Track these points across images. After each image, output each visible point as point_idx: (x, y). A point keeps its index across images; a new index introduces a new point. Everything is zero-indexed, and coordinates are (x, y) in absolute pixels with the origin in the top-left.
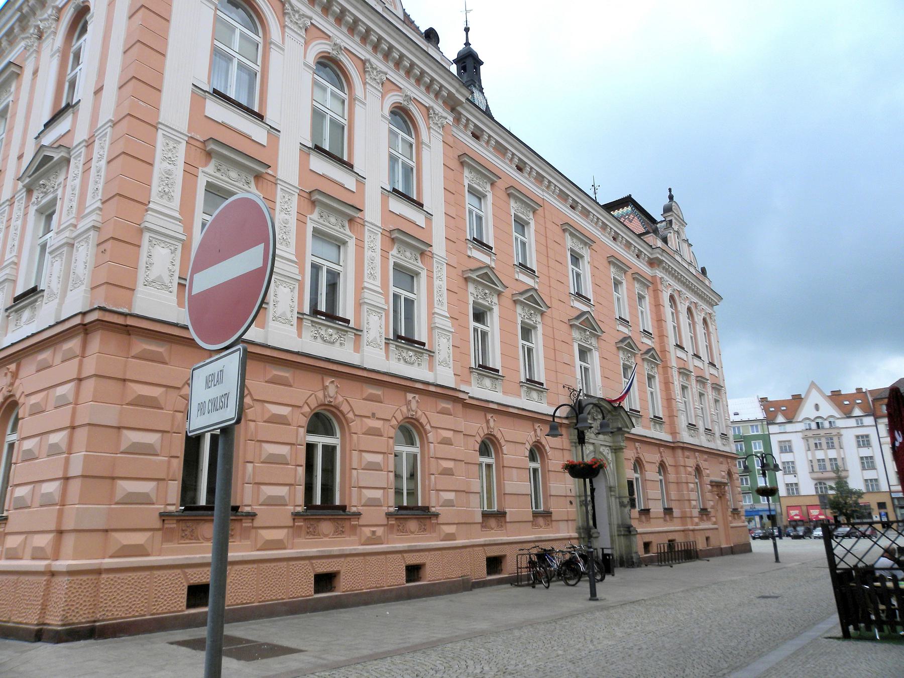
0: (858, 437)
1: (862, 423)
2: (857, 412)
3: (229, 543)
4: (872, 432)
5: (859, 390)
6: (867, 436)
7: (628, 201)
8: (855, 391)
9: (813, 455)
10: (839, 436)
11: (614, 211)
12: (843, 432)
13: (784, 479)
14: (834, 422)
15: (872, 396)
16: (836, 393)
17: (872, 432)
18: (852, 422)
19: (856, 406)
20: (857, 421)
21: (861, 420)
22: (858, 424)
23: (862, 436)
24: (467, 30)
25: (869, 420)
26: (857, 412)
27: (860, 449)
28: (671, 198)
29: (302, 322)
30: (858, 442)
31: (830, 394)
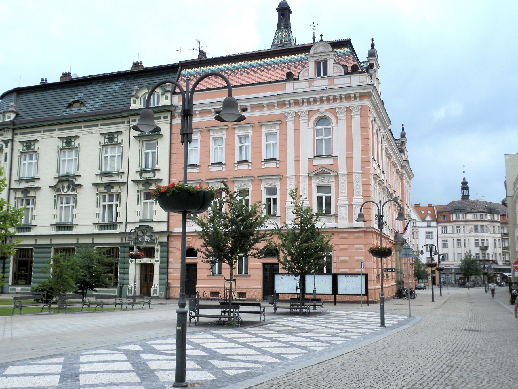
0: (426, 233)
1: (430, 225)
2: (428, 218)
3: (179, 285)
4: (434, 230)
5: (430, 205)
6: (432, 233)
7: (347, 43)
8: (427, 205)
9: (416, 241)
10: (417, 231)
11: (337, 49)
12: (419, 229)
13: (157, 298)
14: (415, 223)
15: (437, 209)
16: (417, 206)
17: (434, 230)
18: (425, 224)
19: (428, 215)
20: (427, 223)
21: (430, 223)
22: (428, 225)
23: (429, 233)
24: (464, 172)
25: (434, 224)
26: (428, 218)
27: (427, 240)
28: (373, 45)
29: (311, 180)
30: (427, 235)
31: (414, 206)
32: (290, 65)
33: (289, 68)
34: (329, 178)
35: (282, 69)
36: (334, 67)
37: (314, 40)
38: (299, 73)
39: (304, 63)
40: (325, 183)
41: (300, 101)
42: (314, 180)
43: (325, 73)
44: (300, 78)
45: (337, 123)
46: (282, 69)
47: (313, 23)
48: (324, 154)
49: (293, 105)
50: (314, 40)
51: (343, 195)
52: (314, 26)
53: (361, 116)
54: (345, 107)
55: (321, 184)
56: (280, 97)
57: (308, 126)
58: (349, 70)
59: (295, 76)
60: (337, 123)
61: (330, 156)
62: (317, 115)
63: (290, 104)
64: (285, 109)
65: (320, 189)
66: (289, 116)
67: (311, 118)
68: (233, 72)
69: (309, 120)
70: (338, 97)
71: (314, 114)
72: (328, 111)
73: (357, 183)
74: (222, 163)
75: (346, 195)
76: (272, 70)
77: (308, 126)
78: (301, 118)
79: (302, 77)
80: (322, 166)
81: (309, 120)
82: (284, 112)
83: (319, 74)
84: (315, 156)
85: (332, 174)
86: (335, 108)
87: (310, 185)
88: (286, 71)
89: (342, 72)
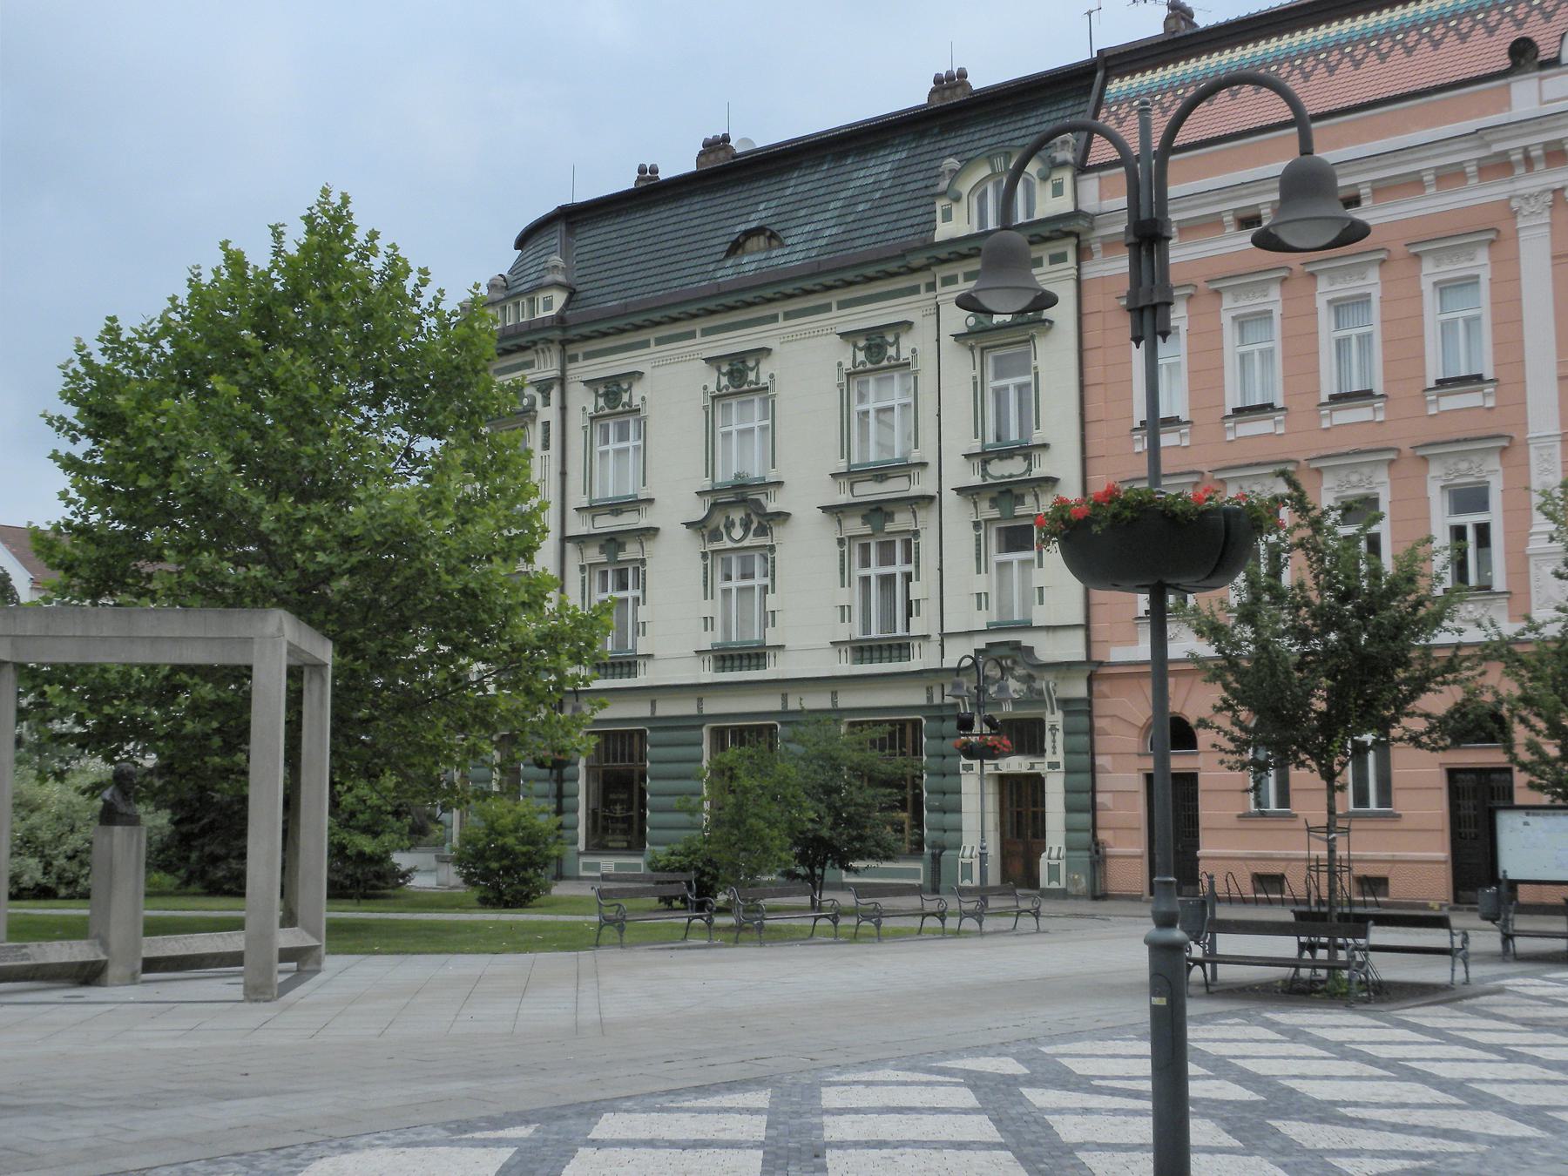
33: (1519, 24)
46: (1491, 31)
59: (1545, 53)
64: (1512, 182)
76: (1452, 38)
88: (1509, 34)
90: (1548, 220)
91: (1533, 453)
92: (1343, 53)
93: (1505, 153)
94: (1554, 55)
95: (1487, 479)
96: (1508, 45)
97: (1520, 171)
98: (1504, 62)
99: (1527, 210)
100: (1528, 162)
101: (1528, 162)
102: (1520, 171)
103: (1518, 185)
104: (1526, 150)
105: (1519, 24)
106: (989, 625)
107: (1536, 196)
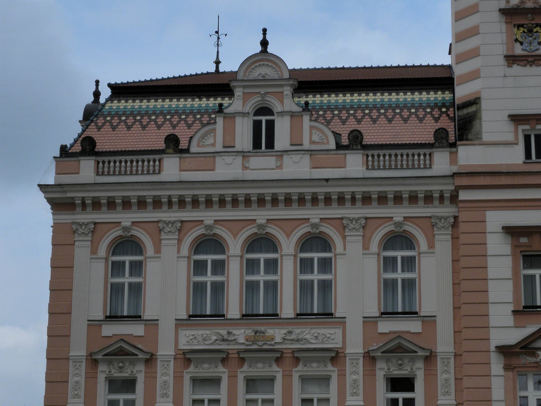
32: (175, 119)
33: (174, 127)
34: (134, 365)
35: (159, 127)
36: (311, 127)
37: (217, 67)
38: (191, 138)
39: (205, 119)
40: (126, 374)
41: (165, 200)
42: (102, 368)
43: (270, 144)
44: (193, 149)
45: (345, 249)
46: (159, 127)
47: (217, 32)
48: (261, 312)
49: (191, 206)
50: (217, 67)
51: (355, 398)
52: (218, 38)
53: (452, 238)
54: (90, 223)
55: (397, 373)
56: (65, 189)
57: (179, 251)
58: (345, 141)
59: (183, 145)
60: (345, 249)
61: (136, 317)
62: (198, 232)
63: (442, 198)
64: (74, 214)
65: (198, 382)
66: (81, 231)
67: (185, 235)
68: (153, 120)
69: (180, 241)
70: (348, 197)
71: (380, 225)
72: (224, 226)
73: (76, 379)
74: (140, 317)
75: (361, 397)
76: (122, 126)
77: (179, 251)
78: (163, 236)
79: (198, 146)
80: (399, 335)
81: (180, 241)
82: (70, 221)
83: (257, 144)
84: (107, 317)
85: (421, 353)
86: (342, 219)
87: (91, 378)
88: (167, 130)
89: (328, 143)
90: (177, 237)
91: (159, 364)
92: (165, 119)
93: (73, 198)
94: (187, 147)
95: (136, 376)
96: (164, 137)
97: (79, 209)
98: (161, 145)
99: (81, 231)
100: (170, 203)
101: (353, 200)
102: (79, 209)
103: (77, 217)
104: (83, 198)
105: (174, 127)
106: (390, 331)
107: (173, 223)
